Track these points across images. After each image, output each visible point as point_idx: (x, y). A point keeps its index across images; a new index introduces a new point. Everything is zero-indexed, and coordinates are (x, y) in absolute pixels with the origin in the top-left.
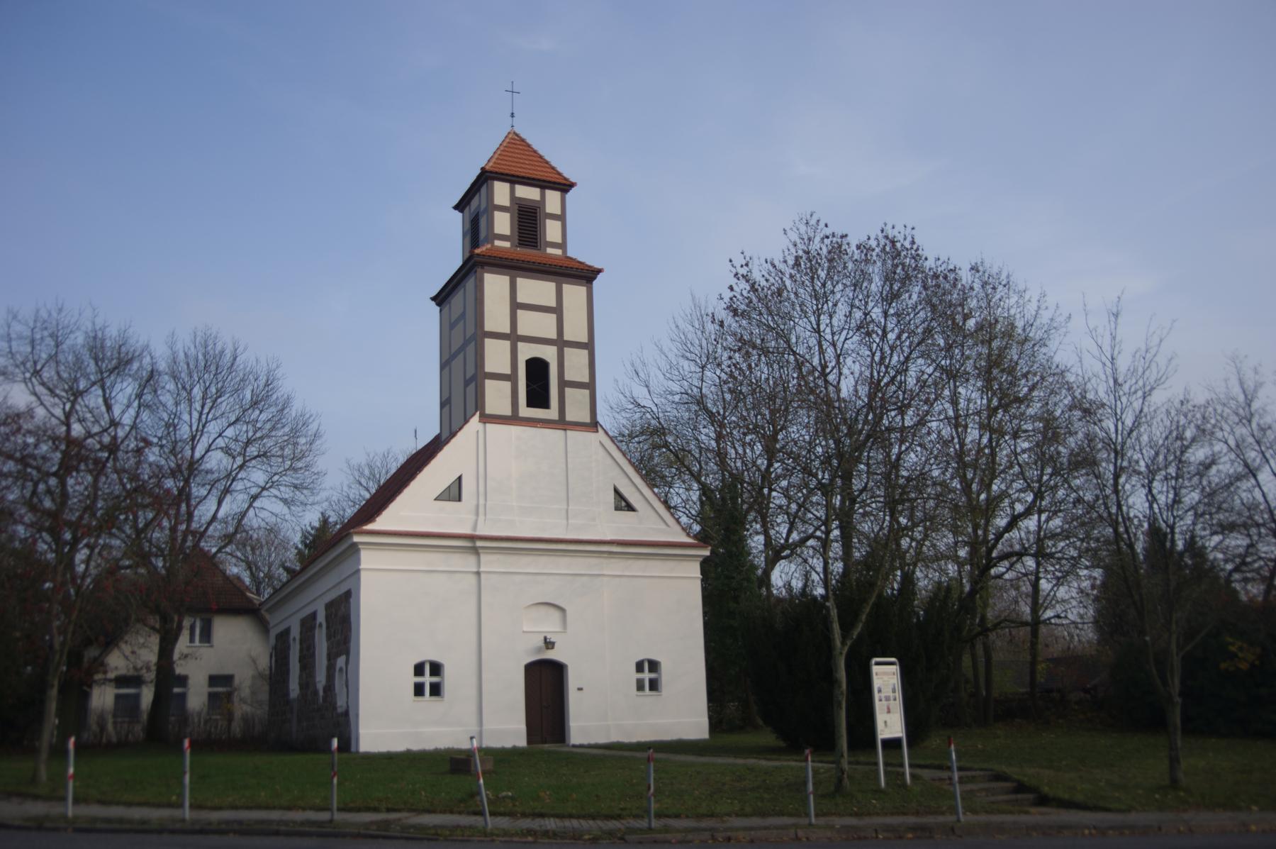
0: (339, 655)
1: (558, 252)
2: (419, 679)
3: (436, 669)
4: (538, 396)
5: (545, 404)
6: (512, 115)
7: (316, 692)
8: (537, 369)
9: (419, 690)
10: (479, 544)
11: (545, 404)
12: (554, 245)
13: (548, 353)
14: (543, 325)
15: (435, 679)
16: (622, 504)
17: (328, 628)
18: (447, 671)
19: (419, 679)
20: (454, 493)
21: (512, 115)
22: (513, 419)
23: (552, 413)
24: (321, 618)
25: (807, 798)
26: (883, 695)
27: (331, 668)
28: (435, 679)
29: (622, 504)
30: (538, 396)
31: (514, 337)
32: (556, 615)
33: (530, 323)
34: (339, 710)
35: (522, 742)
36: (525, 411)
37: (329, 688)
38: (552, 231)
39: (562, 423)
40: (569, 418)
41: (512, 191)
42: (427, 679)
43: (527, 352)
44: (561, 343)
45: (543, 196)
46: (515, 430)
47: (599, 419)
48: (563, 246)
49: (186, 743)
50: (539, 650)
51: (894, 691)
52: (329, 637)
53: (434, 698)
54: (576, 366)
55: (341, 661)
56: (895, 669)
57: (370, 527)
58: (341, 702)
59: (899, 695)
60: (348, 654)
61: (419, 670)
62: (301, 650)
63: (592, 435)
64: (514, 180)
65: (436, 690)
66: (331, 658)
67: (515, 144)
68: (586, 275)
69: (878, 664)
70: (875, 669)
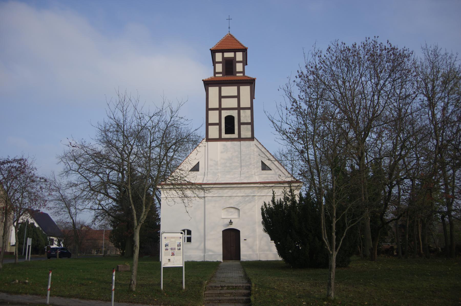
1: (242, 75)
3: (189, 232)
4: (230, 129)
5: (233, 132)
6: (229, 28)
8: (230, 120)
10: (203, 186)
11: (233, 132)
12: (239, 72)
13: (234, 113)
14: (233, 103)
15: (189, 236)
16: (265, 167)
21: (229, 28)
22: (220, 139)
23: (236, 136)
25: (111, 292)
28: (189, 236)
29: (265, 167)
30: (230, 129)
31: (220, 109)
32: (237, 211)
33: (226, 103)
35: (220, 259)
36: (224, 136)
38: (239, 67)
39: (240, 139)
40: (242, 136)
41: (223, 55)
43: (225, 114)
44: (239, 109)
45: (235, 55)
46: (219, 143)
47: (255, 136)
48: (243, 72)
50: (228, 225)
53: (188, 243)
54: (245, 116)
63: (252, 143)
64: (223, 51)
67: (230, 38)
68: (251, 82)
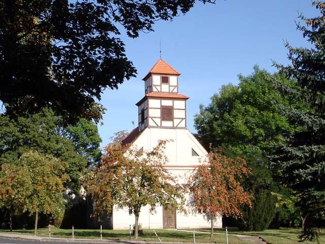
29: (194, 153)
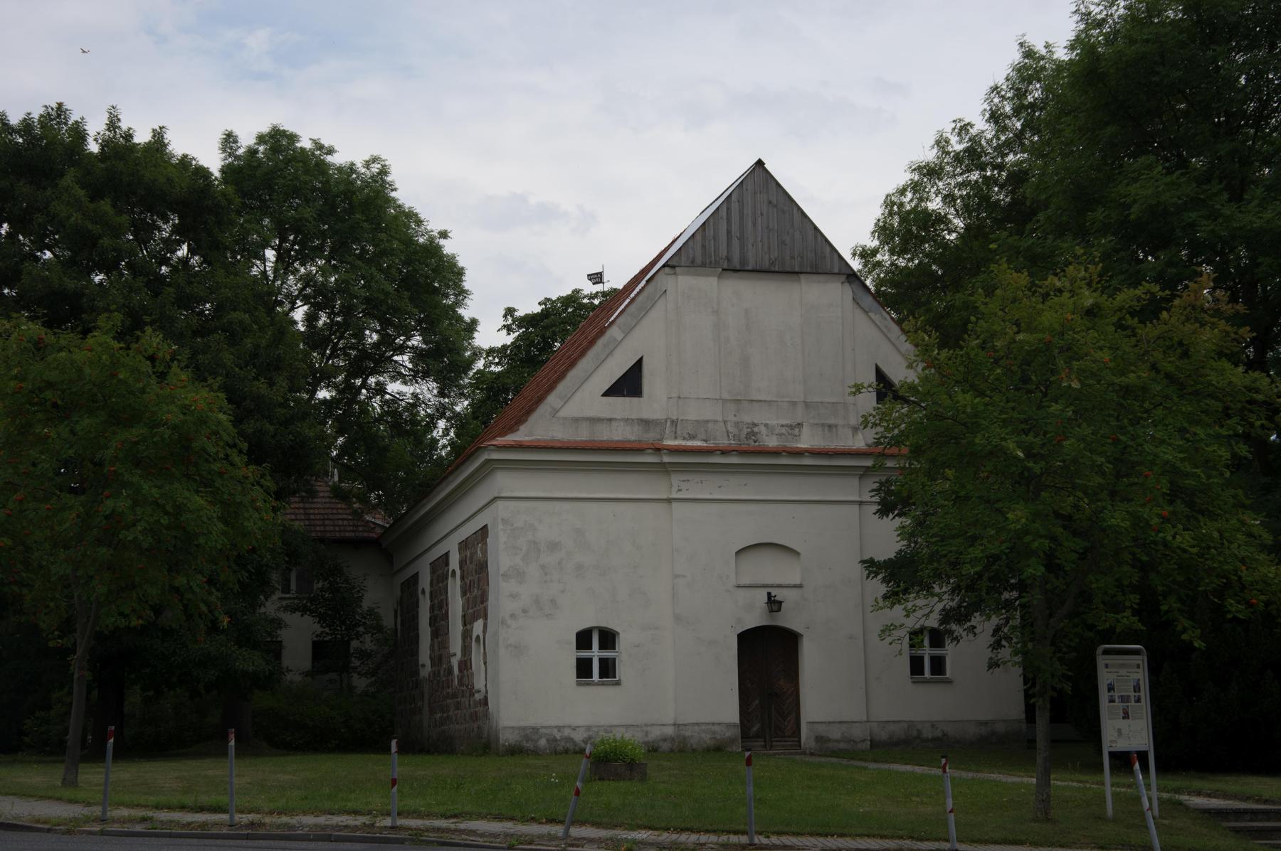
0: (475, 618)
2: (584, 654)
3: (609, 639)
7: (450, 671)
9: (583, 669)
17: (462, 578)
18: (623, 642)
19: (607, 654)
20: (629, 384)
24: (454, 563)
26: (1116, 695)
27: (467, 635)
34: (477, 696)
37: (465, 665)
42: (595, 653)
49: (394, 743)
51: (1137, 688)
52: (464, 593)
55: (478, 627)
56: (1142, 660)
57: (511, 438)
58: (479, 684)
59: (1145, 693)
60: (486, 618)
61: (583, 639)
62: (432, 608)
65: (608, 668)
66: (467, 621)
69: (1106, 652)
70: (1101, 661)
